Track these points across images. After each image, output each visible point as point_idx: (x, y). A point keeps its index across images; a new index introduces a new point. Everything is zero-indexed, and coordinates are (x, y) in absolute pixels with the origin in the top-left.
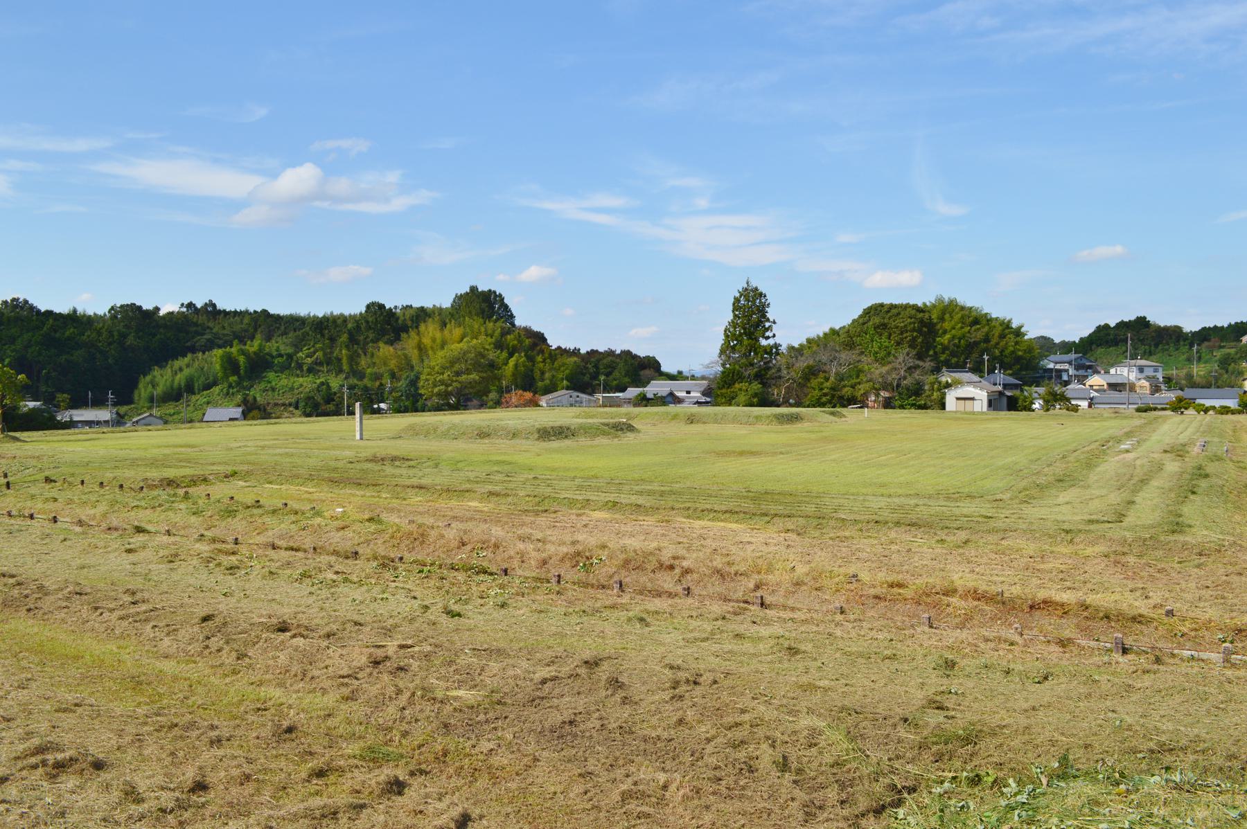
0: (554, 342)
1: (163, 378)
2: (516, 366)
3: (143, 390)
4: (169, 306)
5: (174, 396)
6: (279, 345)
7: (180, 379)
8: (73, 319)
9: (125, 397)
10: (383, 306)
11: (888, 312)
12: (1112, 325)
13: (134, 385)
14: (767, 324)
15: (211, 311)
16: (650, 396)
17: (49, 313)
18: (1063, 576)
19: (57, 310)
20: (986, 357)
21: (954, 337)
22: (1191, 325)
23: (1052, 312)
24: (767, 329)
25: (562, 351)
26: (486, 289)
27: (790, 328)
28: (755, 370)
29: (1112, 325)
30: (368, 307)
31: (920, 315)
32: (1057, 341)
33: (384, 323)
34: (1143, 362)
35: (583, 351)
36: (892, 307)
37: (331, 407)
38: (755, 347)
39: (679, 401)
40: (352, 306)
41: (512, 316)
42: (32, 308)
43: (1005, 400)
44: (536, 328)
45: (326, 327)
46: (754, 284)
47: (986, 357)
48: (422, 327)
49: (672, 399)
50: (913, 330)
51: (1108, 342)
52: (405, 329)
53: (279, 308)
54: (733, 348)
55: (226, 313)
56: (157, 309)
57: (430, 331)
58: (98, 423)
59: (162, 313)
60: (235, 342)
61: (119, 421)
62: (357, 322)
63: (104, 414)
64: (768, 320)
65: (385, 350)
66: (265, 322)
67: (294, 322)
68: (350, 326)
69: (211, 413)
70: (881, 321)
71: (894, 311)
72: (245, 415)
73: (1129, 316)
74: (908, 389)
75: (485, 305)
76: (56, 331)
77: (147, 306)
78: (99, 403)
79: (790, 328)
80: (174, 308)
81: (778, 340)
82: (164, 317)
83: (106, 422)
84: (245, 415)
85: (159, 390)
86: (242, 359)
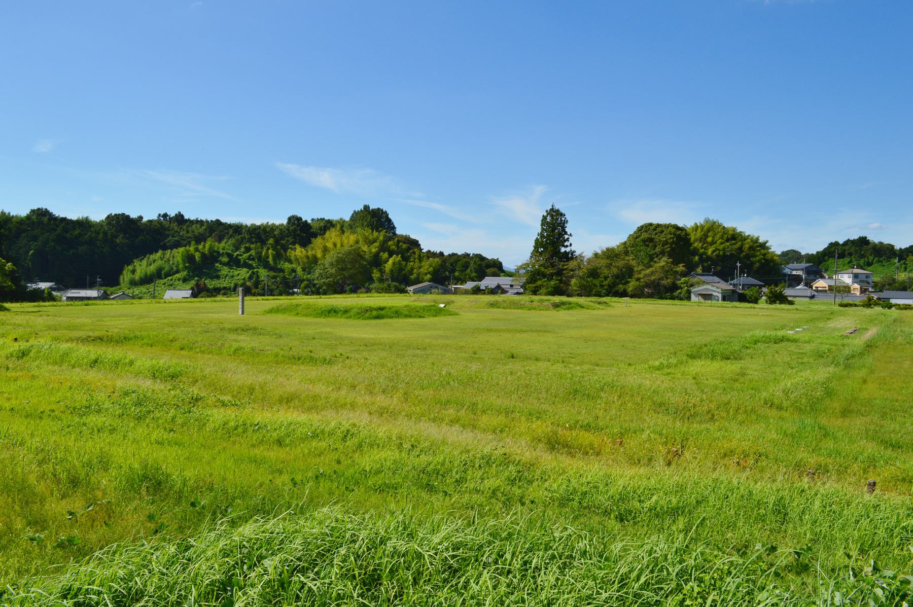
0: (425, 246)
1: (142, 267)
2: (394, 264)
3: (126, 276)
4: (149, 215)
5: (147, 280)
6: (224, 246)
7: (153, 268)
8: (84, 224)
9: (113, 281)
10: (301, 219)
11: (655, 229)
12: (841, 242)
13: (120, 272)
14: (566, 237)
16: (482, 287)
17: (64, 219)
19: (69, 217)
20: (739, 265)
21: (716, 249)
22: (900, 244)
23: (787, 234)
24: (565, 241)
25: (431, 254)
26: (376, 207)
27: (586, 242)
28: (554, 267)
29: (841, 242)
30: (290, 219)
31: (679, 232)
32: (803, 253)
33: (301, 231)
34: (856, 271)
35: (446, 254)
36: (659, 225)
37: (259, 290)
38: (556, 252)
39: (504, 292)
40: (280, 219)
41: (394, 228)
42: (50, 214)
43: (736, 296)
44: (413, 237)
45: (259, 234)
46: (556, 207)
47: (739, 265)
48: (327, 234)
49: (498, 290)
50: (673, 243)
51: (838, 254)
52: (315, 235)
53: (227, 219)
54: (541, 254)
55: (191, 222)
56: (141, 218)
57: (332, 236)
58: (89, 298)
59: (145, 220)
61: (105, 297)
62: (281, 230)
63: (93, 293)
64: (566, 233)
65: (298, 252)
66: (217, 229)
67: (237, 229)
68: (276, 233)
70: (649, 237)
71: (659, 229)
72: (194, 295)
73: (855, 237)
74: (665, 287)
75: (376, 219)
76: (67, 232)
77: (134, 215)
78: (91, 286)
79: (586, 242)
80: (154, 217)
81: (573, 248)
82: (145, 224)
83: (95, 298)
84: (194, 295)
85: (137, 276)
86: (197, 256)
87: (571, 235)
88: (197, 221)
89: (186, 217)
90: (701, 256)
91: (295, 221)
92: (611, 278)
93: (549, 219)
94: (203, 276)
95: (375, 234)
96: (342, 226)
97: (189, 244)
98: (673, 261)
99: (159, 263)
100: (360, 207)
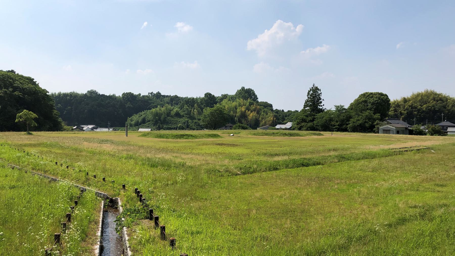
1: (136, 118)
2: (253, 116)
3: (128, 121)
15: (158, 95)
18: (77, 154)
20: (443, 115)
27: (329, 104)
30: (206, 95)
36: (371, 94)
43: (408, 131)
46: (316, 85)
47: (443, 115)
55: (164, 96)
60: (159, 106)
69: (85, 128)
79: (329, 104)
81: (324, 107)
85: (133, 123)
87: (323, 100)
88: (167, 96)
89: (162, 94)
90: (419, 110)
91: (208, 95)
92: (341, 121)
93: (311, 92)
94: (161, 123)
95: (245, 101)
96: (232, 98)
97: (157, 107)
98: (372, 113)
99: (143, 116)
100: (240, 88)
